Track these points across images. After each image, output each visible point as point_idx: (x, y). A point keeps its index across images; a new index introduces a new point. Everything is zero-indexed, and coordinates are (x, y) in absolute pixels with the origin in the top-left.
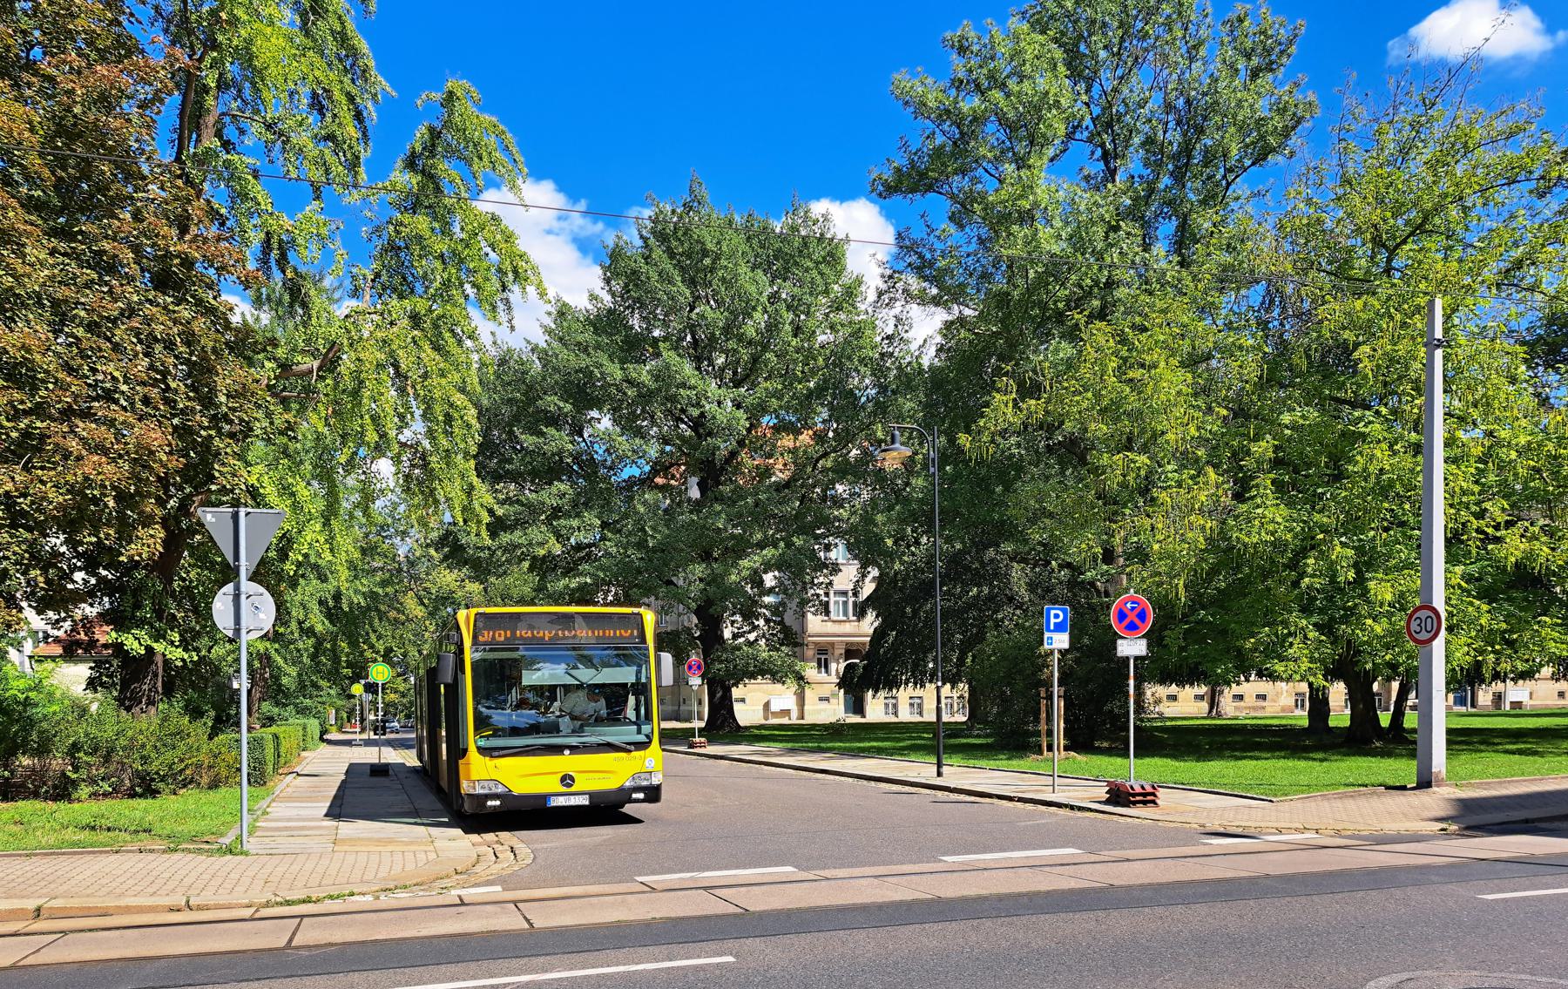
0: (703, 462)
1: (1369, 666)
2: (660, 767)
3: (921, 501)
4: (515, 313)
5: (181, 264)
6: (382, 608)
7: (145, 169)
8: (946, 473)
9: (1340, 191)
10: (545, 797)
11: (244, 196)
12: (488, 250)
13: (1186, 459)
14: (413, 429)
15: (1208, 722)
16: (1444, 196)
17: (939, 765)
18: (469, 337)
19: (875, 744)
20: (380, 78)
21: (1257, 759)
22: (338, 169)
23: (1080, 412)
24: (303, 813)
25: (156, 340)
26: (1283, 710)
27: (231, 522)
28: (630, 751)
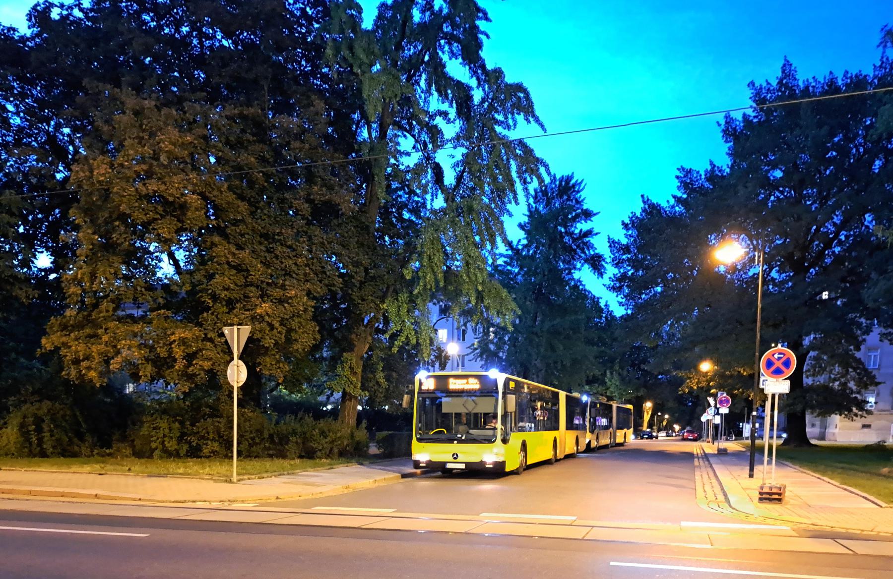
10: (445, 463)
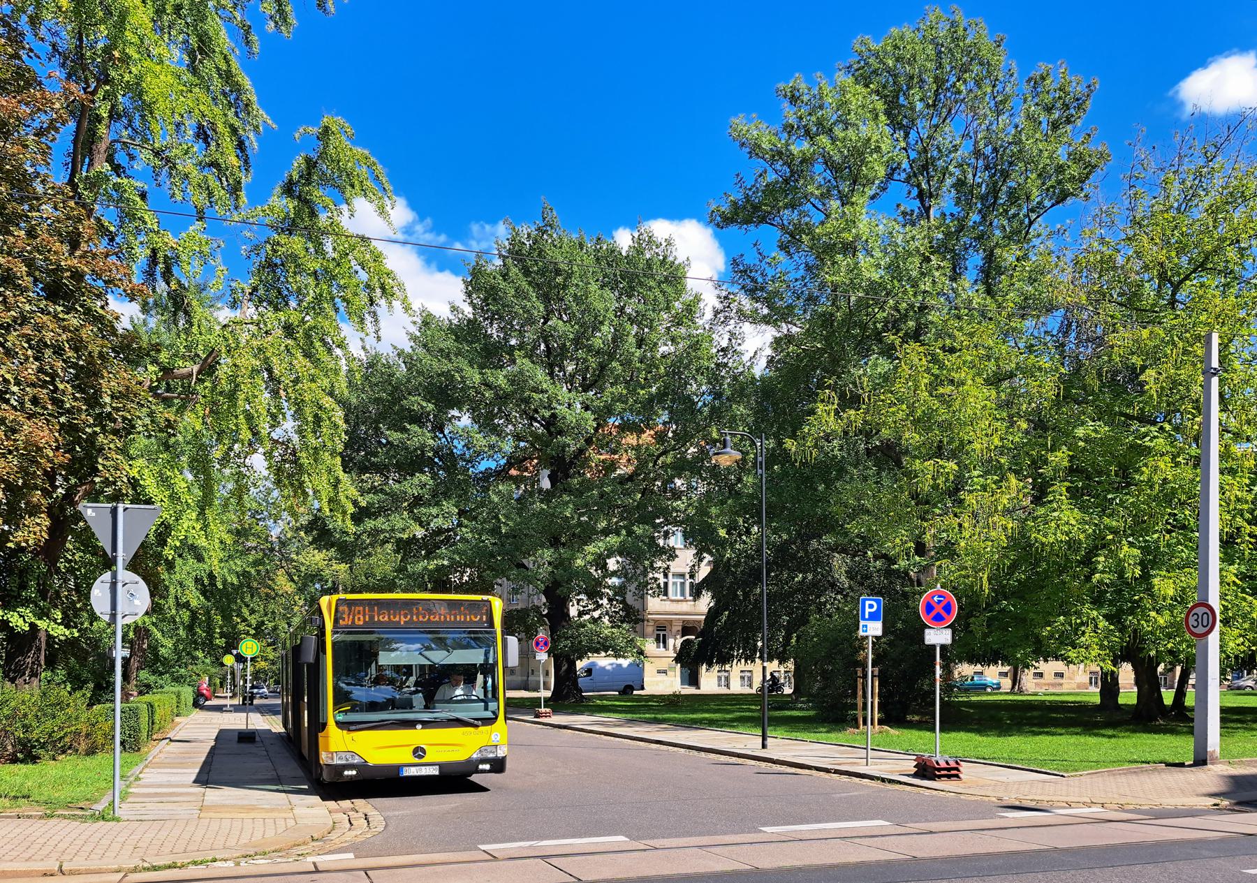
0: (553, 457)
1: (1153, 653)
2: (505, 741)
3: (751, 496)
4: (382, 324)
5: (71, 277)
6: (255, 584)
7: (40, 189)
8: (774, 472)
9: (1130, 233)
10: (398, 768)
11: (133, 217)
12: (358, 268)
13: (991, 467)
14: (284, 427)
15: (1011, 697)
16: (1222, 240)
17: (764, 738)
18: (338, 346)
19: (707, 715)
20: (261, 112)
21: (1053, 734)
22: (220, 193)
23: (895, 422)
24: (174, 779)
25: (46, 345)
26: (1079, 687)
27: (110, 516)
28: (477, 726)
